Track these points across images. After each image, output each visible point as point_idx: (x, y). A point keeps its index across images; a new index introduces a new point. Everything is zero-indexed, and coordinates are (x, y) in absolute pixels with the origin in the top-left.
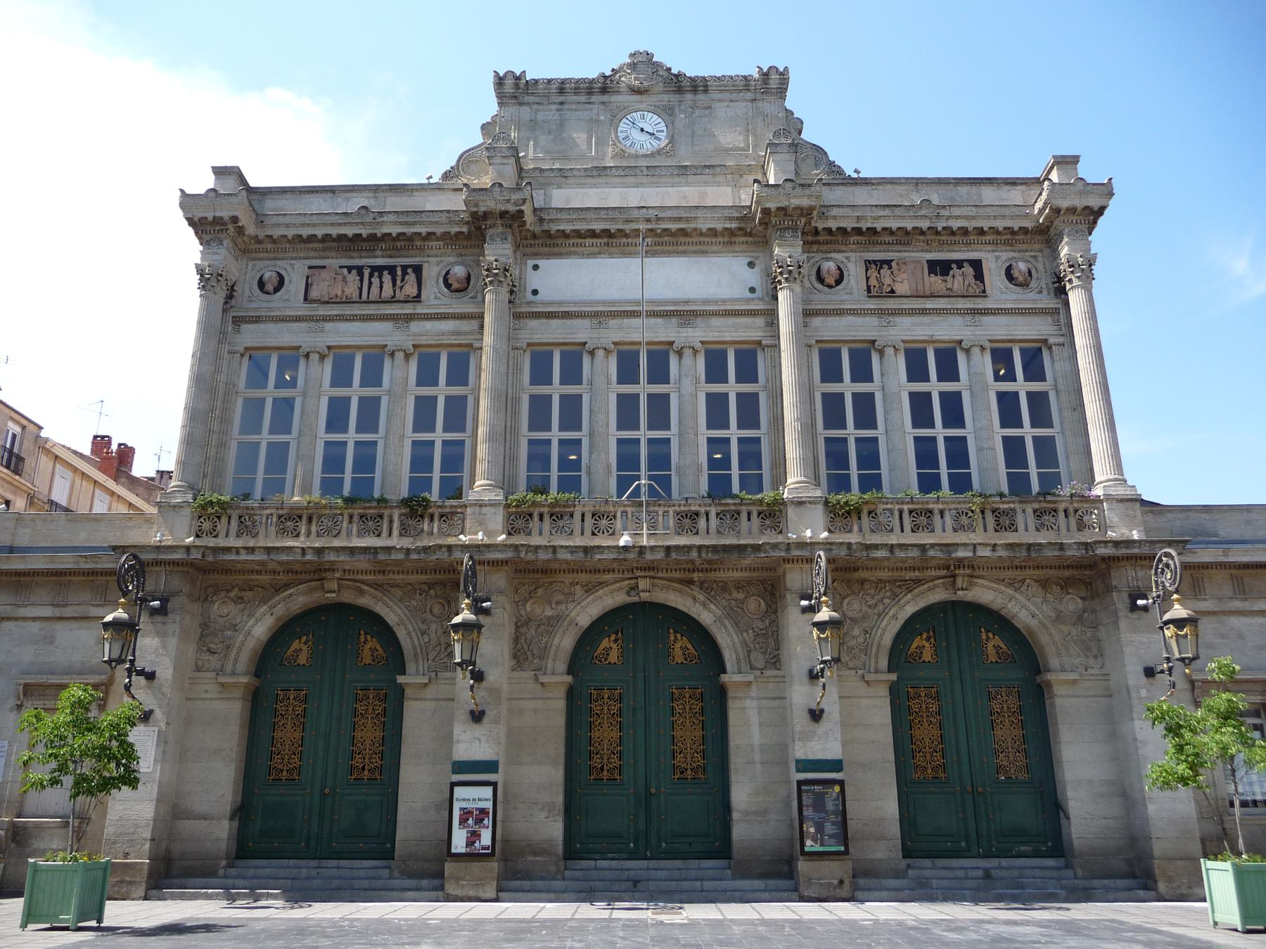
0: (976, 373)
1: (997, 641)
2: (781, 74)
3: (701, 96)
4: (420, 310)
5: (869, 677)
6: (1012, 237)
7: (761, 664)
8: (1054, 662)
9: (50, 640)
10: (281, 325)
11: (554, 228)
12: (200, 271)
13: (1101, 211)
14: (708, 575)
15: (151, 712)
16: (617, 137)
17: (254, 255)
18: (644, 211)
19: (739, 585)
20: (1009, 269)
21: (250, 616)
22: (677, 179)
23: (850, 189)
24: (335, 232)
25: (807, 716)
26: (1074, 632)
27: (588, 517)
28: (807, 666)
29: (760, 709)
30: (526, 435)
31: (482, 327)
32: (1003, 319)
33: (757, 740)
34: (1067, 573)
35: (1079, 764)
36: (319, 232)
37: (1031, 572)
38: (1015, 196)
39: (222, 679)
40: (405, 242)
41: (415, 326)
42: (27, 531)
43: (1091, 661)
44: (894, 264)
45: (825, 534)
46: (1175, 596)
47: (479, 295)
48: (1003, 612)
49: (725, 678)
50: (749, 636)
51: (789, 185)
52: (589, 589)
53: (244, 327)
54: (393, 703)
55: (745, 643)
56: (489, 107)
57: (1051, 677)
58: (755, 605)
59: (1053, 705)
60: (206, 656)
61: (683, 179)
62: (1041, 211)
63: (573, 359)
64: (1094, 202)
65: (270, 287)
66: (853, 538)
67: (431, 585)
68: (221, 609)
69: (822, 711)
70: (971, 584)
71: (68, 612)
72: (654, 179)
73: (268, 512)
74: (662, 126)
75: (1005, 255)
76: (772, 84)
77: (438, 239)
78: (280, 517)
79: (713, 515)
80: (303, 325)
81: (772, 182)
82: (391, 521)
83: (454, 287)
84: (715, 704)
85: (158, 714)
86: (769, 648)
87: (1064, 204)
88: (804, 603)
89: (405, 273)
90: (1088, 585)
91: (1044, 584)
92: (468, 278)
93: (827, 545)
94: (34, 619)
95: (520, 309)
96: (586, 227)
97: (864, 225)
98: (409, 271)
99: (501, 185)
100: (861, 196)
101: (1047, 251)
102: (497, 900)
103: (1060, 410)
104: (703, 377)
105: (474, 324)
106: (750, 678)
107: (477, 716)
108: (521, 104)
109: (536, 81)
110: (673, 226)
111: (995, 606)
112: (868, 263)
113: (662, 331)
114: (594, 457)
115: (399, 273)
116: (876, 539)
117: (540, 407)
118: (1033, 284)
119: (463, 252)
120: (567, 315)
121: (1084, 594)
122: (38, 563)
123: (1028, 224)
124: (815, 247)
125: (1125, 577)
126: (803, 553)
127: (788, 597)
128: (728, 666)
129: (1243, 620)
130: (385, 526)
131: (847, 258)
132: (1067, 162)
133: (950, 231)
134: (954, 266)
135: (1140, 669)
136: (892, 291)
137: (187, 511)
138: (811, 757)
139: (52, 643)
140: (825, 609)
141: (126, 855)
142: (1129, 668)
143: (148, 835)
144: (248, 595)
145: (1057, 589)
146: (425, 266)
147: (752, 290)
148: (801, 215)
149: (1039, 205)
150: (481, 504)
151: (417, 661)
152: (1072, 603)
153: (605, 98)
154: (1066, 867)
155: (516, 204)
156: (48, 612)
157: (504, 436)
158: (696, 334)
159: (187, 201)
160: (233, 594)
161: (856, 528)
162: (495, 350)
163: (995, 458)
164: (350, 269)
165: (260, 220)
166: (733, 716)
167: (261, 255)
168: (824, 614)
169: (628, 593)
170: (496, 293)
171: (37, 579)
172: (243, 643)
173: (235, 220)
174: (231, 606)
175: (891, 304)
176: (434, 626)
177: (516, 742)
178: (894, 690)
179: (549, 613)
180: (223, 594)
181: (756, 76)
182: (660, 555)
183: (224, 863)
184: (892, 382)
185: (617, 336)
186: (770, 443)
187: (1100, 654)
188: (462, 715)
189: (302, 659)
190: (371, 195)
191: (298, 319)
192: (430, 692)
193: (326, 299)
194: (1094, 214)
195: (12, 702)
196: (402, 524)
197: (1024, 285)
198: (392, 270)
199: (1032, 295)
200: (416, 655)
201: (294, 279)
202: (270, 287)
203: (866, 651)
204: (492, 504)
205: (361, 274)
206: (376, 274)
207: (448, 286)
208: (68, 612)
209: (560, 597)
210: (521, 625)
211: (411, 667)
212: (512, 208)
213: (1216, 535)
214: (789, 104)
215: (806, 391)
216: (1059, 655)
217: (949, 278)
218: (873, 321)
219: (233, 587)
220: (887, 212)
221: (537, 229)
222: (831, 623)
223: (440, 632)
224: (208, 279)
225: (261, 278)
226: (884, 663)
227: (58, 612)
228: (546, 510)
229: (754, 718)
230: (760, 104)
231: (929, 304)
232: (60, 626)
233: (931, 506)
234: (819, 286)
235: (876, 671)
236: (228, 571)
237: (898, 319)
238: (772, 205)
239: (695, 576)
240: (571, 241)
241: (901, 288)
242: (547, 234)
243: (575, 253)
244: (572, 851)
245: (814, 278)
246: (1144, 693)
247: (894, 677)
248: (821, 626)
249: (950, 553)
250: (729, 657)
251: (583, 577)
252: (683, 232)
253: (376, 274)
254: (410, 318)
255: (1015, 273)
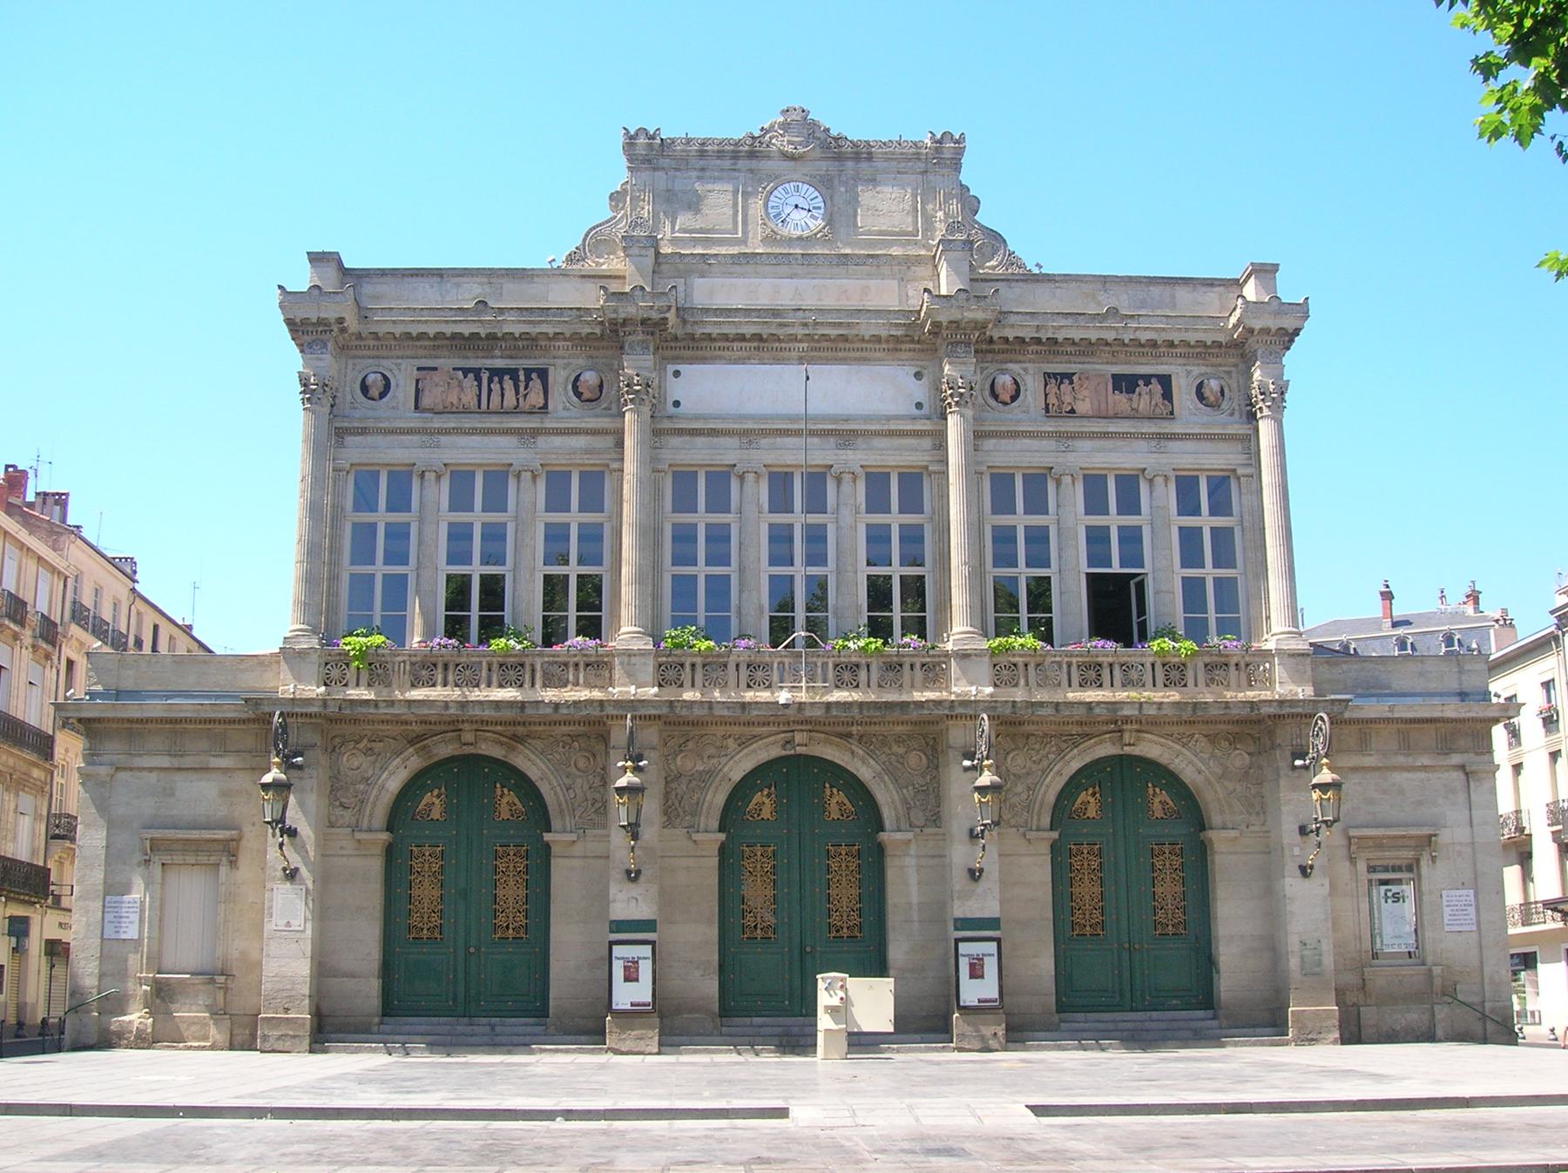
0: (1160, 500)
1: (1164, 796)
2: (957, 142)
3: (864, 165)
4: (549, 424)
5: (1030, 835)
6: (1202, 351)
7: (921, 822)
8: (1216, 819)
9: (169, 792)
10: (390, 438)
11: (699, 331)
12: (305, 383)
13: (1297, 332)
14: (867, 728)
15: (297, 869)
16: (767, 214)
17: (354, 352)
18: (800, 313)
19: (899, 740)
20: (1200, 386)
21: (383, 769)
22: (836, 270)
23: (1030, 286)
24: (448, 330)
25: (965, 874)
26: (1239, 788)
27: (743, 668)
28: (967, 826)
29: (919, 868)
30: (669, 570)
31: (620, 444)
32: (1190, 445)
33: (915, 900)
34: (1236, 729)
35: (1233, 919)
36: (432, 330)
37: (1201, 727)
38: (1210, 304)
39: (358, 835)
40: (531, 342)
41: (542, 442)
42: (131, 673)
43: (1253, 819)
44: (1075, 378)
45: (989, 690)
46: (1325, 760)
47: (614, 406)
48: (1171, 767)
49: (883, 836)
50: (908, 793)
51: (963, 296)
52: (744, 742)
53: (349, 440)
54: (539, 863)
55: (905, 801)
56: (618, 173)
57: (1211, 834)
58: (916, 760)
59: (1213, 862)
60: (339, 811)
61: (842, 270)
62: (1236, 326)
63: (720, 479)
64: (1288, 323)
65: (374, 392)
66: (1019, 695)
67: (574, 737)
68: (353, 762)
69: (981, 871)
70: (1138, 739)
71: (188, 762)
72: (810, 269)
73: (400, 659)
74: (819, 202)
75: (1197, 370)
76: (940, 159)
77: (565, 339)
78: (412, 664)
79: (874, 668)
80: (416, 438)
81: (944, 292)
82: (533, 671)
83: (585, 396)
84: (874, 861)
85: (304, 871)
86: (930, 808)
87: (1257, 325)
88: (967, 763)
89: (528, 379)
90: (1256, 740)
91: (1212, 739)
92: (601, 386)
93: (991, 705)
94: (151, 769)
95: (664, 426)
96: (734, 331)
97: (1044, 336)
98: (534, 376)
99: (642, 288)
100: (1045, 301)
101: (1241, 366)
102: (659, 1053)
103: (1244, 549)
104: (863, 506)
105: (609, 441)
106: (910, 835)
107: (633, 876)
108: (655, 169)
109: (673, 141)
110: (833, 332)
111: (1164, 761)
112: (1048, 375)
113: (822, 454)
114: (745, 596)
115: (522, 378)
116: (1039, 696)
117: (684, 536)
118: (1225, 405)
119: (595, 353)
120: (713, 433)
121: (1252, 749)
122: (155, 708)
123: (1222, 338)
124: (989, 356)
125: (1285, 734)
126: (965, 711)
127: (951, 753)
128: (887, 823)
129: (1406, 775)
130: (527, 676)
131: (1025, 370)
132: (1265, 272)
133: (1137, 343)
134: (1141, 382)
135: (1296, 827)
136: (1072, 411)
137: (314, 657)
138: (969, 916)
139: (172, 795)
140: (986, 773)
141: (287, 1010)
142: (1285, 827)
143: (307, 992)
144: (378, 746)
145: (1224, 744)
146: (551, 369)
147: (919, 406)
148: (975, 328)
149: (1233, 320)
150: (629, 654)
151: (563, 818)
152: (1239, 759)
153: (754, 164)
154: (1213, 1018)
155: (660, 310)
156: (165, 761)
157: (649, 576)
158: (857, 458)
159: (288, 298)
160: (361, 746)
161: (1022, 682)
162: (640, 481)
163: (1173, 601)
164: (466, 371)
165: (364, 315)
166: (891, 875)
167: (361, 353)
168: (986, 779)
169: (784, 747)
170: (636, 411)
171: (149, 726)
172: (377, 798)
173: (341, 321)
174: (362, 758)
175: (1070, 426)
176: (579, 781)
177: (666, 898)
178: (1055, 848)
179: (700, 767)
180: (352, 744)
181: (928, 141)
182: (819, 713)
183: (377, 1020)
184: (1069, 516)
185: (770, 458)
186: (935, 583)
187: (1263, 810)
188: (617, 875)
189: (436, 814)
190: (485, 280)
191: (410, 431)
192: (578, 849)
193: (440, 407)
194: (1288, 337)
195: (138, 857)
196: (545, 674)
197: (1214, 406)
198: (513, 373)
199: (1223, 418)
200: (561, 811)
201: (401, 383)
202: (374, 392)
203: (1028, 809)
204: (642, 653)
205: (478, 379)
206: (496, 379)
207: (578, 395)
208: (188, 762)
209: (712, 751)
210: (670, 780)
211: (556, 823)
212: (655, 315)
213: (1389, 687)
214: (964, 178)
215: (975, 528)
216: (1222, 812)
217: (1135, 397)
218: (1050, 444)
219: (362, 738)
220: (1069, 322)
221: (680, 333)
222: (993, 788)
223: (586, 787)
224: (312, 391)
225: (364, 380)
226: (1046, 820)
227: (176, 762)
228: (699, 660)
229: (913, 877)
230: (931, 177)
231: (1112, 427)
232: (178, 777)
233: (1100, 659)
234: (992, 402)
235: (1038, 830)
236: (356, 721)
237: (1079, 444)
238: (943, 318)
239: (854, 729)
240: (718, 345)
241: (1083, 407)
242: (692, 337)
243: (720, 358)
244: (726, 1011)
245: (987, 393)
246: (1296, 851)
247: (1055, 835)
248: (982, 790)
249: (1115, 711)
250: (888, 815)
251: (736, 729)
252: (844, 338)
253: (496, 379)
254: (535, 433)
255: (1207, 393)
